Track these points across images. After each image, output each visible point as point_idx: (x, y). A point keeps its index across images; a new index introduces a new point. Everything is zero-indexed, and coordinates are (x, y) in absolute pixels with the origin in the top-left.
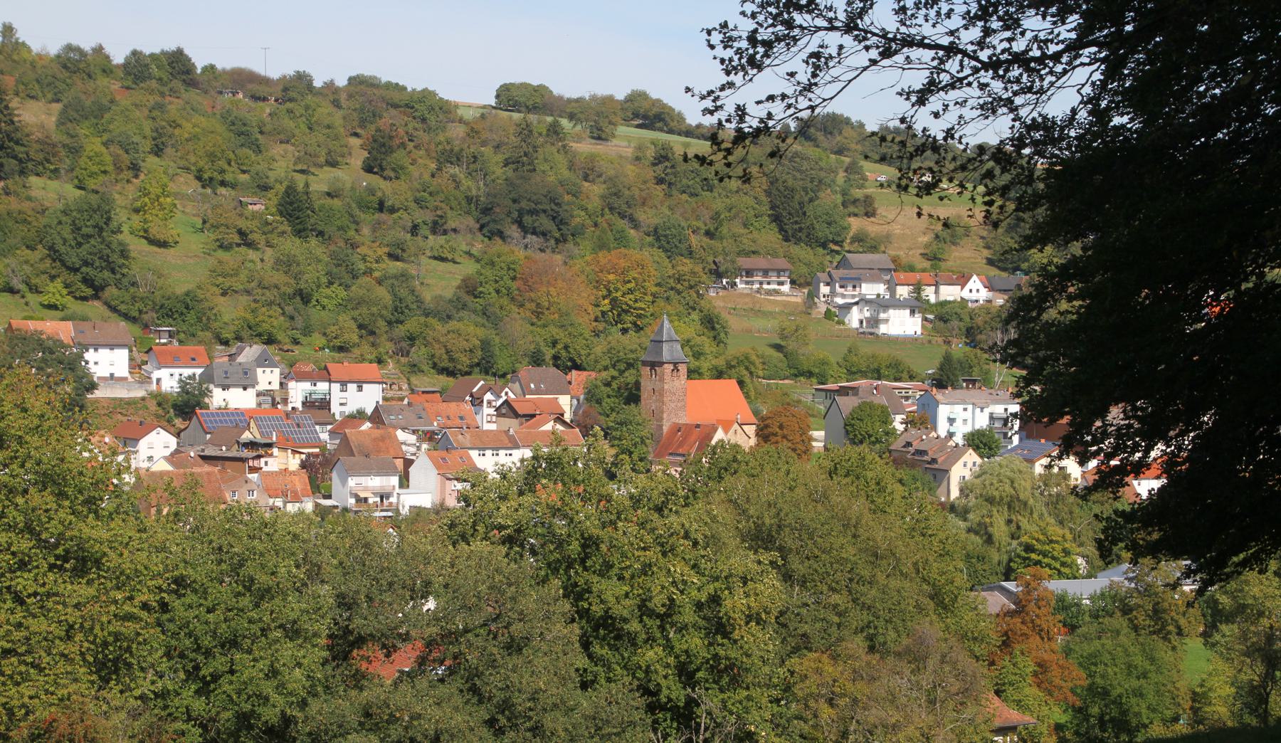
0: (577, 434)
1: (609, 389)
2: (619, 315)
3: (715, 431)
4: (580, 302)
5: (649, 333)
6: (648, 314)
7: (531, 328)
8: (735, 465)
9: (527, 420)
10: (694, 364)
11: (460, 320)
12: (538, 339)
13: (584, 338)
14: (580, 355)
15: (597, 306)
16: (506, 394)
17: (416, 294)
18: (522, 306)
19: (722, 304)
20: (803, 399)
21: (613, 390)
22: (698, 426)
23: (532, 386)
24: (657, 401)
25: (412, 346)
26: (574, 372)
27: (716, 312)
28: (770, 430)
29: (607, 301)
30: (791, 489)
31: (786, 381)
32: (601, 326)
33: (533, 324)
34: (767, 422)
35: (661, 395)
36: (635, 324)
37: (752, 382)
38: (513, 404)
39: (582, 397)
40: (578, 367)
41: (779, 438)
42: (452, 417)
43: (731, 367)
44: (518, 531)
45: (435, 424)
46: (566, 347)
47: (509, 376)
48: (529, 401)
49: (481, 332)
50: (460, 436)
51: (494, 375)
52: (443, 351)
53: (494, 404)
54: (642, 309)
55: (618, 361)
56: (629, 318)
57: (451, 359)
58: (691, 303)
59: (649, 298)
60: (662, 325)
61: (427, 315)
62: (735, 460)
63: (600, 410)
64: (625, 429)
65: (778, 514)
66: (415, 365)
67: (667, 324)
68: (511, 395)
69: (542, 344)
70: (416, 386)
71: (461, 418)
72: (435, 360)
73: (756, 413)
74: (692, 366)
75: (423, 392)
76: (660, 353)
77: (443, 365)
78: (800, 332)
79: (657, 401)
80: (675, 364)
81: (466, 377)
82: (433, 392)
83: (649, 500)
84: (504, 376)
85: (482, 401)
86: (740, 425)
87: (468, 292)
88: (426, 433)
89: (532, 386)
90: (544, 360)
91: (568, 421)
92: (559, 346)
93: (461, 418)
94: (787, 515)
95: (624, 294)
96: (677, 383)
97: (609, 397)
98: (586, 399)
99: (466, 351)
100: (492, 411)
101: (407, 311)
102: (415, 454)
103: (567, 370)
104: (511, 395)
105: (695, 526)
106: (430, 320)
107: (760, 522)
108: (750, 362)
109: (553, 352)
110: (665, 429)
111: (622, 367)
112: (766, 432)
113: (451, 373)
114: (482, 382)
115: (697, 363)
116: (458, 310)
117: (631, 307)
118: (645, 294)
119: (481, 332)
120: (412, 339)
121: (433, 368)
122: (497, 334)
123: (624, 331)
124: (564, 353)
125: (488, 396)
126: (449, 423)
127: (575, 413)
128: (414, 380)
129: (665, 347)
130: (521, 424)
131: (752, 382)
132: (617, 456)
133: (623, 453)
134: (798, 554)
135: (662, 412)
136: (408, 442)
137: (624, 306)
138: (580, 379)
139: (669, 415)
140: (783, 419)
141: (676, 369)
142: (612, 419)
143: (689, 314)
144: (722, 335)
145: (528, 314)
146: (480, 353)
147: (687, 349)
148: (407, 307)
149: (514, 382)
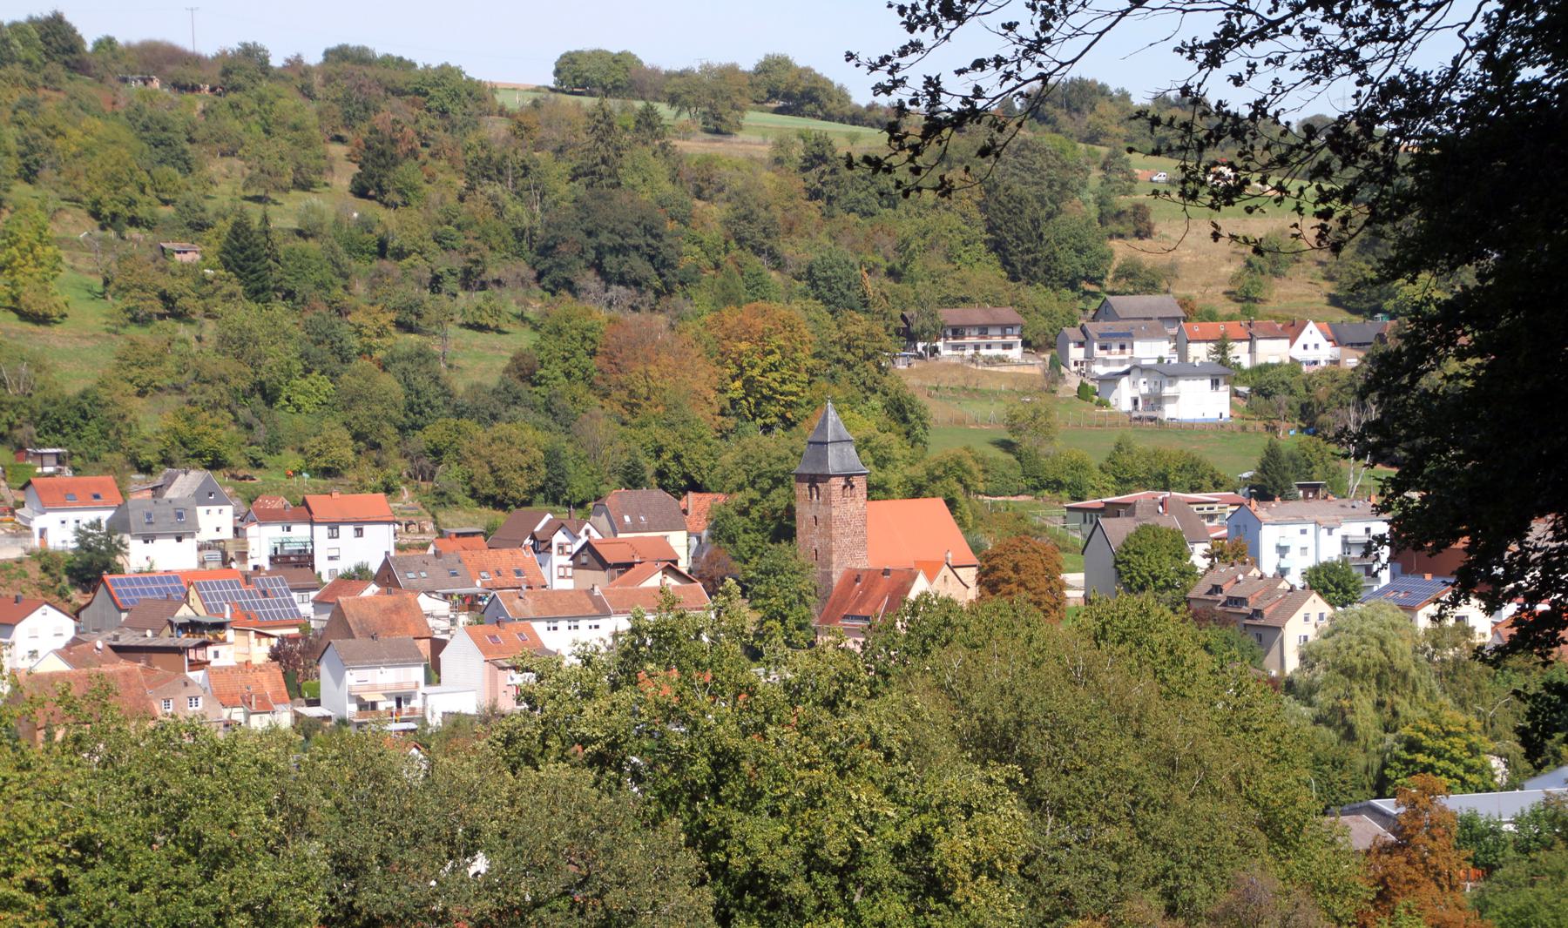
1: (746, 520)
2: (758, 404)
3: (914, 578)
4: (697, 386)
5: (806, 430)
6: (803, 402)
7: (622, 429)
8: (948, 631)
10: (877, 476)
11: (511, 420)
12: (633, 445)
14: (700, 469)
15: (723, 391)
16: (587, 532)
17: (442, 382)
18: (606, 395)
19: (917, 382)
21: (753, 520)
22: (886, 572)
23: (627, 519)
24: (821, 535)
25: (438, 463)
26: (691, 494)
27: (908, 393)
28: (999, 574)
29: (738, 384)
31: (1022, 498)
32: (730, 423)
33: (624, 424)
34: (993, 562)
35: (828, 526)
36: (783, 417)
37: (968, 501)
39: (705, 534)
40: (697, 487)
41: (1014, 587)
42: (503, 571)
44: (613, 745)
45: (478, 583)
47: (590, 505)
48: (623, 542)
49: (544, 438)
50: (518, 601)
51: (568, 504)
52: (487, 469)
53: (568, 549)
54: (792, 394)
55: (759, 476)
56: (772, 408)
57: (500, 483)
59: (804, 377)
61: (459, 415)
62: (947, 623)
63: (734, 553)
66: (442, 494)
67: (832, 416)
68: (595, 535)
70: (446, 525)
71: (518, 573)
72: (474, 484)
73: (976, 548)
74: (874, 480)
75: (458, 535)
76: (823, 460)
79: (821, 535)
80: (848, 477)
81: (524, 509)
82: (474, 534)
83: (814, 690)
85: (550, 546)
86: (952, 568)
87: (522, 378)
88: (464, 598)
89: (627, 519)
90: (643, 479)
91: (685, 571)
93: (518, 573)
94: (1031, 705)
95: (764, 371)
96: (851, 506)
97: (745, 531)
98: (712, 536)
99: (521, 468)
100: (566, 560)
101: (428, 410)
102: (447, 632)
103: (679, 492)
104: (595, 535)
106: (466, 423)
107: (989, 718)
108: (964, 471)
110: (836, 578)
111: (766, 483)
112: (993, 577)
113: (500, 505)
114: (549, 516)
115: (882, 475)
117: (775, 392)
119: (544, 438)
120: (437, 453)
121: (472, 497)
124: (673, 466)
125: (559, 537)
126: (500, 581)
127: (695, 559)
129: (832, 451)
130: (612, 579)
131: (968, 501)
132: (762, 622)
133: (771, 618)
134: (1049, 765)
135: (830, 552)
136: (437, 613)
139: (841, 556)
140: (1019, 557)
141: (849, 484)
144: (919, 430)
145: (617, 407)
146: (544, 471)
147: (865, 452)
149: (599, 515)
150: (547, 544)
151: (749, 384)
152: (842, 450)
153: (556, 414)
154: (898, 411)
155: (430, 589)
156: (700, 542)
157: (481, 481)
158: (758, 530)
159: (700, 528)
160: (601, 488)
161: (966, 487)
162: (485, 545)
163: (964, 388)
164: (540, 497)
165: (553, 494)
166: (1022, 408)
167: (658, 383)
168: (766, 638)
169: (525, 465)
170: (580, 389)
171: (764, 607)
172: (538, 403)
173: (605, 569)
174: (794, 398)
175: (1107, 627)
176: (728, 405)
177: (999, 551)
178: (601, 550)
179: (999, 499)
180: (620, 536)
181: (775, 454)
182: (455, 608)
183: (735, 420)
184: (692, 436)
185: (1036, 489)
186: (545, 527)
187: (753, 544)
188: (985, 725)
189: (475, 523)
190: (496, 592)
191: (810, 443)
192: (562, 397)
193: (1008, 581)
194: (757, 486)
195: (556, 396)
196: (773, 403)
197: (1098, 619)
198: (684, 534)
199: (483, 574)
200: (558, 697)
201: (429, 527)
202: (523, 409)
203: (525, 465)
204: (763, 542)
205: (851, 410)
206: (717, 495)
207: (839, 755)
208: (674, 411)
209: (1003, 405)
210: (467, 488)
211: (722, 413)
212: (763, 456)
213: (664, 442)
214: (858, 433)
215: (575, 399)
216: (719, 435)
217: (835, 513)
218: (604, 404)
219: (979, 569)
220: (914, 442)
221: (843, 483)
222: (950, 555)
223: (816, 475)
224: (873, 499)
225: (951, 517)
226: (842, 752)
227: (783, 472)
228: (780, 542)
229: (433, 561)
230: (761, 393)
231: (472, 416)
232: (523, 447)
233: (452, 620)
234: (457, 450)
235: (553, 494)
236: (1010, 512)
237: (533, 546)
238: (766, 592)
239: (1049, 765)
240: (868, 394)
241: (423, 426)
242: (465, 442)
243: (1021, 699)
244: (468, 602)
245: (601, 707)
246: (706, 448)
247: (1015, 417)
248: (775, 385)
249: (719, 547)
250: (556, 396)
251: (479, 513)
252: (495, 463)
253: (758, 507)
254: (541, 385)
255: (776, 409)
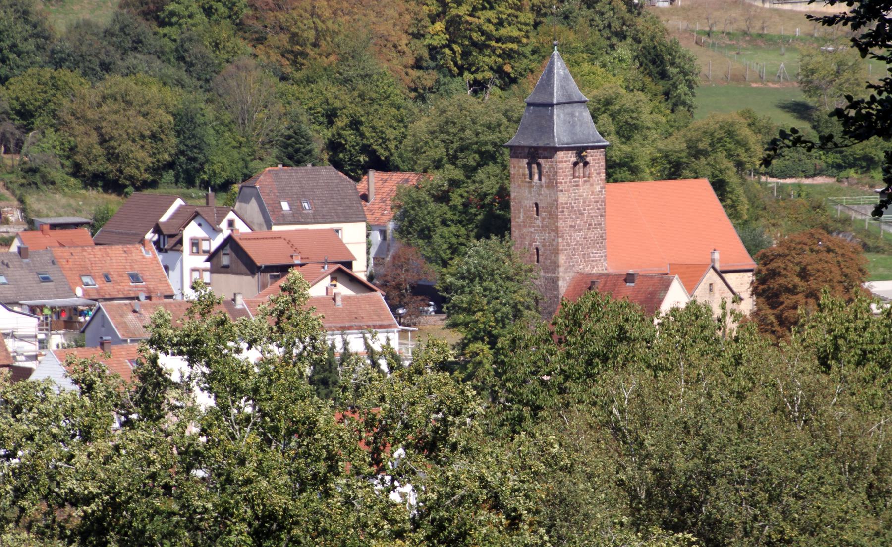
0: (378, 302)
1: (445, 207)
2: (465, 54)
3: (666, 286)
4: (382, 29)
5: (529, 87)
6: (527, 50)
7: (282, 85)
8: (623, 347)
9: (275, 278)
10: (621, 150)
11: (130, 72)
12: (295, 108)
13: (393, 104)
14: (385, 140)
15: (418, 36)
16: (231, 224)
17: (33, 19)
18: (260, 40)
19: (682, 25)
20: (853, 215)
21: (453, 208)
22: (629, 278)
23: (285, 206)
24: (544, 228)
25: (28, 129)
26: (372, 174)
27: (668, 41)
28: (782, 281)
29: (439, 26)
30: (741, 396)
31: (819, 180)
32: (429, 78)
33: (284, 78)
34: (773, 265)
35: (553, 217)
36: (499, 71)
37: (744, 182)
38: (243, 244)
39: (391, 226)
40: (383, 165)
41: (800, 298)
42: (114, 276)
43: (697, 153)
44: (115, 506)
45: (79, 291)
46: (355, 124)
47: (236, 188)
48: (278, 237)
49: (174, 97)
50: (131, 316)
51: (205, 185)
52: (94, 138)
53: (205, 246)
54: (512, 40)
55: (462, 149)
56: (487, 60)
57: (112, 156)
58: (616, 25)
59: (528, 17)
60: (550, 72)
61: (58, 64)
62: (623, 336)
63: (428, 251)
64: (478, 289)
65: (704, 448)
66: (34, 171)
67: (560, 68)
68: (241, 228)
69: (305, 118)
70: (38, 214)
71: (135, 278)
72: (78, 158)
73: (753, 246)
74: (616, 155)
75: (54, 227)
76: (547, 128)
77: (93, 168)
78: (846, 75)
79: (544, 228)
80: (580, 151)
81: (147, 192)
82: (77, 225)
83: (406, 426)
84: (225, 187)
85: (180, 242)
86: (720, 273)
87: (146, 15)
88: (57, 311)
89: (285, 206)
90: (309, 152)
91: (363, 277)
92: (340, 123)
93: (135, 278)
94: (722, 448)
95: (475, 9)
96: (584, 190)
97: (444, 223)
98: (400, 231)
99: (143, 137)
100: (200, 261)
101: (13, 56)
102: (35, 358)
103: (356, 172)
104: (241, 228)
105: (512, 480)
106: (65, 75)
107: (664, 466)
108: (738, 143)
109: (328, 133)
110: (563, 286)
111: (472, 159)
112: (774, 284)
113: (114, 186)
114: (179, 202)
115: (626, 148)
116: (125, 52)
117: (489, 37)
118: (519, 9)
119: (174, 97)
120: (25, 115)
121: (74, 175)
122: (209, 101)
123: (478, 87)
124: (350, 136)
125: (193, 231)
126: (109, 289)
127: (378, 260)
128: (32, 200)
129: (559, 116)
130: (263, 286)
131: (744, 182)
132: (463, 345)
133: (476, 339)
134: (747, 534)
135: (556, 252)
136: (20, 332)
137: (475, 36)
138: (386, 189)
139: (570, 257)
140: (808, 258)
141: (581, 161)
142: (453, 270)
143: (612, 46)
144: (682, 88)
145: (275, 56)
146: (174, 141)
147: (604, 119)
148: (13, 47)
149: (247, 201)
150: (174, 241)
151: (454, 26)
152: (572, 115)
153: (191, 65)
154: (654, 62)
155: (12, 299)
156: (384, 238)
157: (87, 154)
158: (460, 222)
159: (384, 218)
160: (252, 165)
161: (740, 165)
162: (91, 241)
163: (745, 33)
164: (169, 176)
165: (187, 172)
166: (820, 59)
167: (329, 24)
168: (470, 367)
169: (148, 133)
170: (224, 30)
171: (466, 325)
172: (167, 49)
173: (253, 274)
174: (514, 46)
175: (841, 342)
176: (426, 55)
177: (781, 251)
178: (249, 248)
179: (789, 181)
180: (275, 228)
181: (484, 119)
182: (48, 326)
183: (434, 75)
184: (374, 95)
185: (839, 167)
186: (173, 217)
187: (454, 240)
188: (661, 477)
189: (78, 211)
190: (101, 304)
191: (529, 104)
192: (200, 40)
193: (793, 291)
194: (460, 162)
195: (191, 40)
196: (487, 51)
197: (830, 332)
198: (363, 226)
199: (86, 280)
200: (37, 437)
201: (15, 215)
202: (147, 57)
203: (148, 133)
204: (468, 236)
205: (592, 61)
206: (407, 175)
207: (442, 519)
208: (351, 62)
209: (796, 56)
210: (68, 163)
211: (418, 65)
212: (468, 122)
213: (338, 104)
214: (595, 92)
215: (217, 45)
216: (413, 94)
217: (562, 198)
218: (258, 52)
219: (757, 273)
220: (675, 105)
221: (574, 159)
222: (716, 255)
223: (536, 148)
224: (616, 181)
225: (718, 205)
226: (446, 515)
227: (494, 144)
228: (488, 238)
229: (17, 261)
230: (471, 38)
231: (77, 64)
232: (144, 109)
233: (41, 342)
234: (54, 111)
235: (187, 172)
236: (802, 200)
237: (156, 243)
238: (470, 303)
239: (747, 534)
240: (614, 40)
241: (7, 78)
242: (66, 102)
243: (710, 441)
244: (64, 317)
245: (99, 451)
246: (394, 111)
247: (813, 72)
248: (489, 28)
249: (409, 245)
250: (191, 40)
251: (85, 198)
252: (107, 129)
253: (460, 191)
254: (171, 24)
255: (491, 61)
